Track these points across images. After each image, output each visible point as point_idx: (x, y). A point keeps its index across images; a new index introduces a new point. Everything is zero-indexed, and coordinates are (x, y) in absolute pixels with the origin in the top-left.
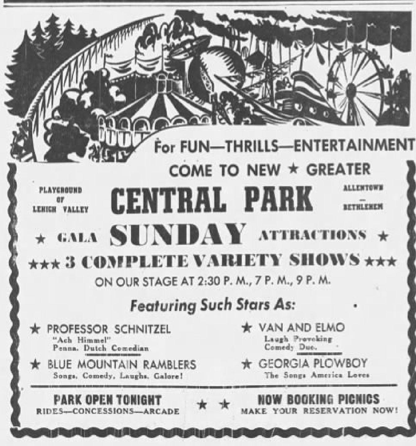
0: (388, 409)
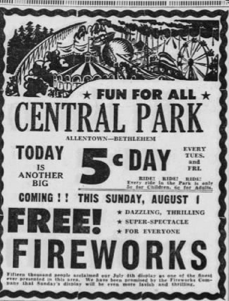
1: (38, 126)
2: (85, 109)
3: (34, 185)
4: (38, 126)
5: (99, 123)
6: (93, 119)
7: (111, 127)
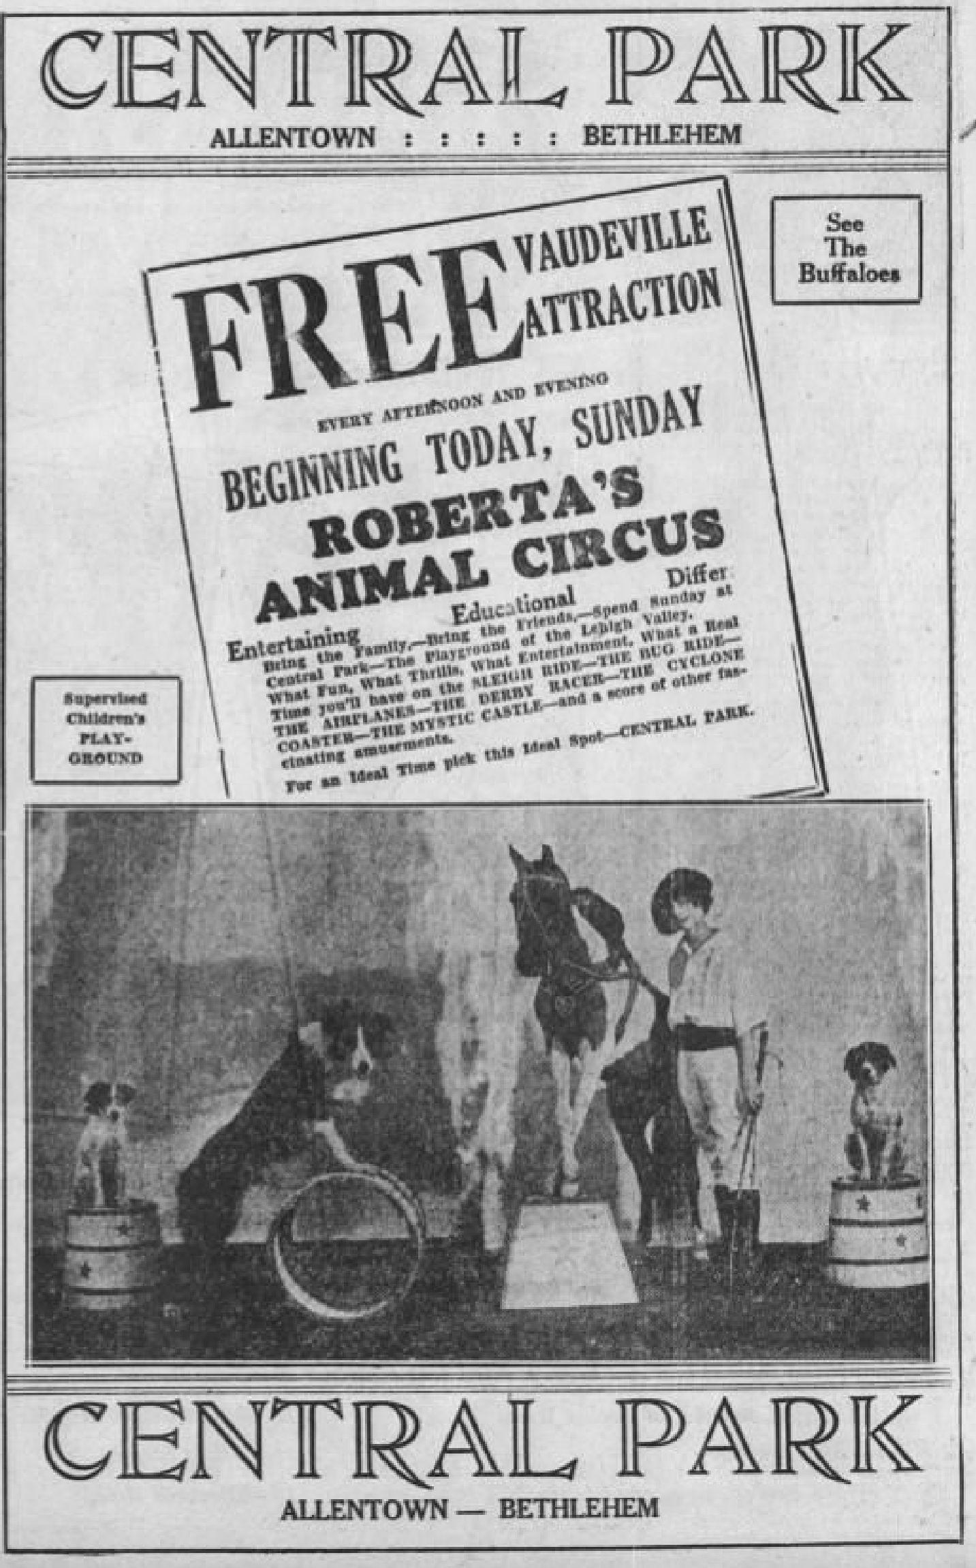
0: (412, 1506)
1: (258, 498)
2: (592, 298)
3: (504, 1516)
4: (258, 498)
5: (612, 312)
6: (605, 308)
7: (628, 313)
